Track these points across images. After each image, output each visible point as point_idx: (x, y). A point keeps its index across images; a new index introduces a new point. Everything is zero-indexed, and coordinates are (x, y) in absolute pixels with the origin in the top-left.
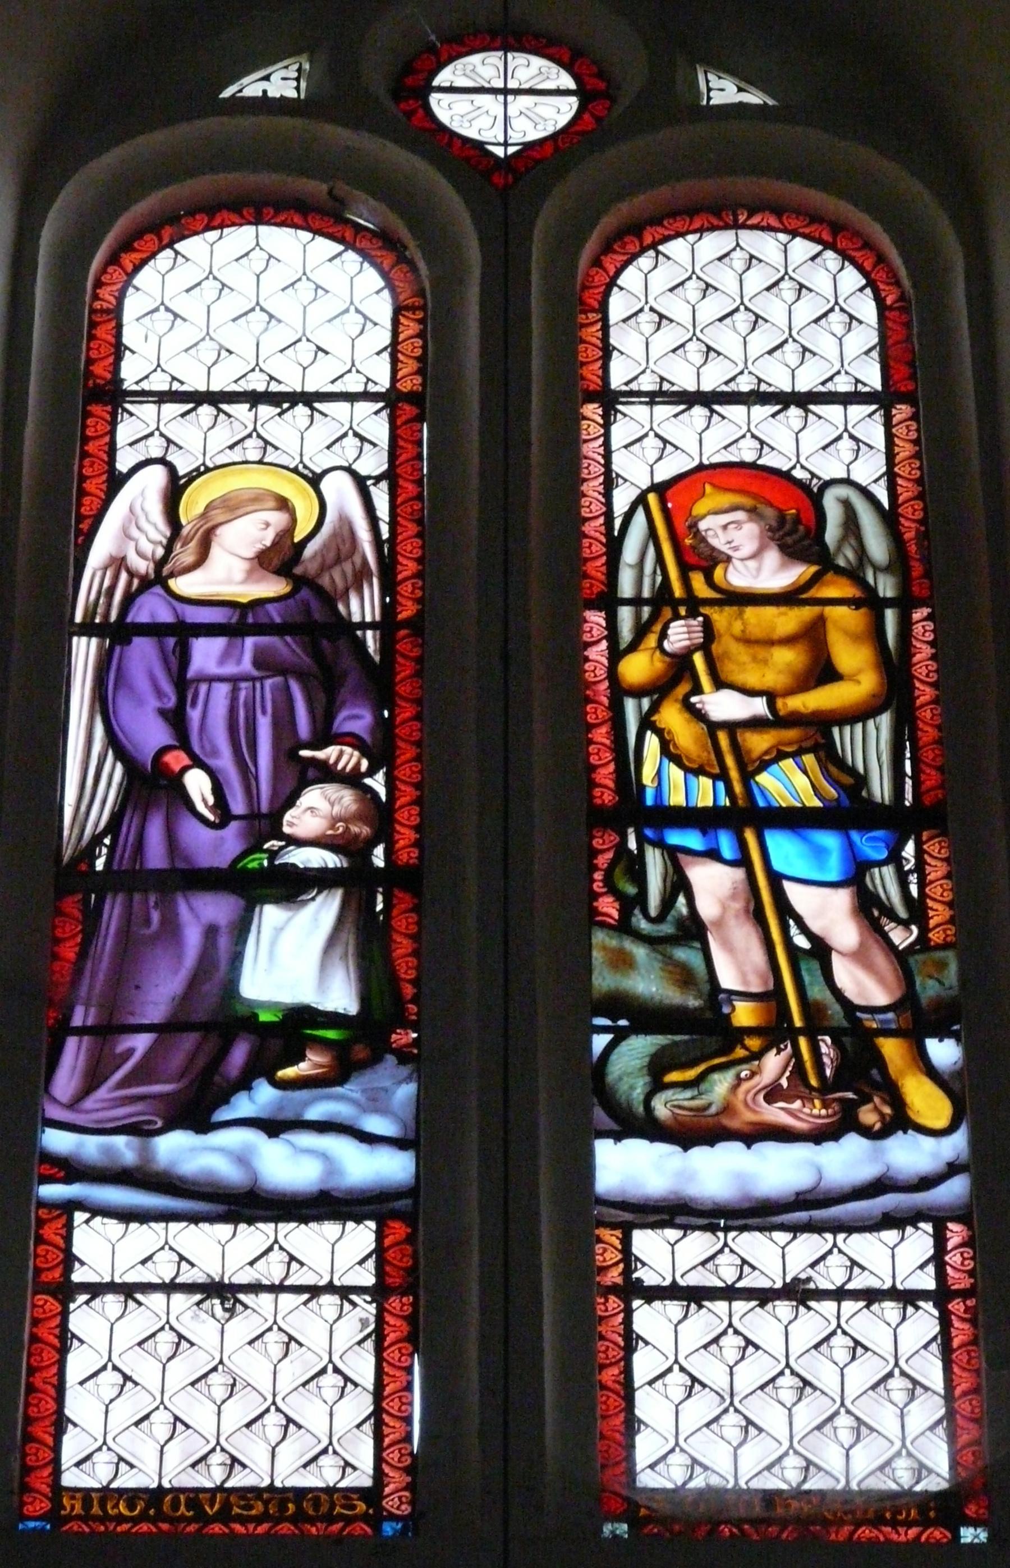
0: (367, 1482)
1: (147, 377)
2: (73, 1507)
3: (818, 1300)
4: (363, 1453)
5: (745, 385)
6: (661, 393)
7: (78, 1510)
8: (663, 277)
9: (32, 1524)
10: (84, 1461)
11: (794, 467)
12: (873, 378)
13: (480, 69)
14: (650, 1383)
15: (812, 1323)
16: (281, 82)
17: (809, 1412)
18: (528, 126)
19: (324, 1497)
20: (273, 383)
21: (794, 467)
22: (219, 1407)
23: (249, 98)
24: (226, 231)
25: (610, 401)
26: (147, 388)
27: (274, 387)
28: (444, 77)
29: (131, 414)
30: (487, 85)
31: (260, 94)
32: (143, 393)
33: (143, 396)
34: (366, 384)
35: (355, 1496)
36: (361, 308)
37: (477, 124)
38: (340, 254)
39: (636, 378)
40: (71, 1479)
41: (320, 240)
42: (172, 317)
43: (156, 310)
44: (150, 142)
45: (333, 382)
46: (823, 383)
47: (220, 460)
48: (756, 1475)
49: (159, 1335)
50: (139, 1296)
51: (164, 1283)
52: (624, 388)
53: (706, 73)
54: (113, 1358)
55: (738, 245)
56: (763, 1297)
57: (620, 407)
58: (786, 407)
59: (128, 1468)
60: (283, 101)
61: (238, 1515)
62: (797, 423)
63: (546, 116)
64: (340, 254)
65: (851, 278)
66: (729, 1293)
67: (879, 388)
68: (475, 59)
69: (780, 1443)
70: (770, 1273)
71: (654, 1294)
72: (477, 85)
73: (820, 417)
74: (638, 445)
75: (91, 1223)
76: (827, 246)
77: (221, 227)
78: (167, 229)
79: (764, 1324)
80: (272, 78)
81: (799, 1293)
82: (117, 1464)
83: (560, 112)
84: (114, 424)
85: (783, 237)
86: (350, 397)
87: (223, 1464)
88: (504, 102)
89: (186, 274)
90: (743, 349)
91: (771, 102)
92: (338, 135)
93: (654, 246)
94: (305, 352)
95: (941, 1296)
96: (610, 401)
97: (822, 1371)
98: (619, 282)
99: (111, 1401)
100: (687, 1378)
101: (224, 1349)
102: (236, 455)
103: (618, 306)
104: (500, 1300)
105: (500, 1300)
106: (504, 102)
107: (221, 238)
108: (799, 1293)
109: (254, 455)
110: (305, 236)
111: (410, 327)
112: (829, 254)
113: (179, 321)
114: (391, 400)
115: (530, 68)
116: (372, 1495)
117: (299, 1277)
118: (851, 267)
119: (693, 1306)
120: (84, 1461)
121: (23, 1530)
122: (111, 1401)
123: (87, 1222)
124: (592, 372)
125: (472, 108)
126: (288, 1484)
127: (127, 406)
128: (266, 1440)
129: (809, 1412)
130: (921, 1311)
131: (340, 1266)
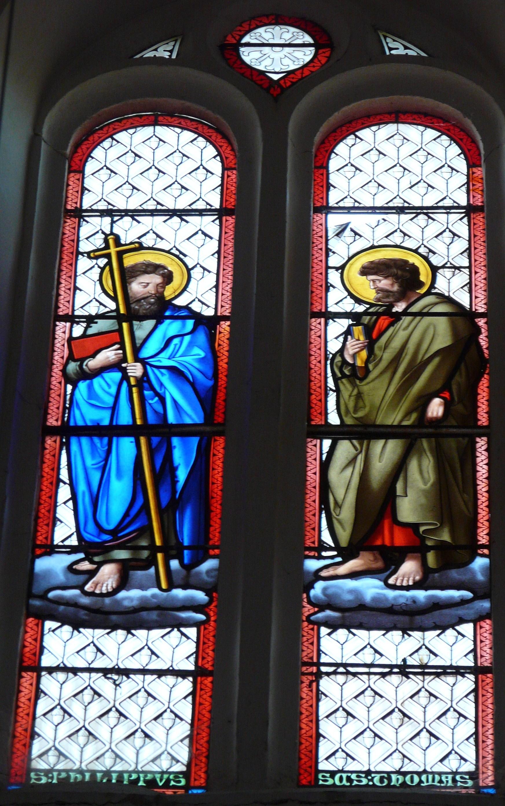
0: (472, 768)
3: (135, 674)
5: (151, 206)
7: (450, 784)
8: (117, 150)
9: (195, 791)
14: (327, 717)
15: (411, 685)
16: (163, 52)
17: (408, 730)
18: (290, 62)
20: (405, 203)
25: (79, 214)
26: (145, 208)
28: (246, 39)
29: (87, 222)
32: (144, 211)
37: (264, 64)
38: (195, 139)
39: (391, 201)
43: (198, 168)
46: (337, 203)
48: (90, 763)
55: (154, 135)
58: (418, 214)
59: (409, 761)
61: (173, 785)
62: (423, 224)
64: (195, 139)
70: (393, 657)
74: (441, 236)
77: (135, 127)
78: (350, 127)
80: (159, 50)
81: (404, 670)
83: (306, 55)
84: (79, 226)
85: (178, 130)
86: (448, 209)
88: (277, 52)
89: (361, 147)
90: (397, 189)
91: (423, 54)
92: (435, 73)
95: (197, 674)
97: (413, 709)
98: (92, 155)
101: (119, 697)
103: (90, 167)
106: (277, 52)
108: (404, 670)
110: (421, 128)
111: (234, 175)
114: (221, 213)
118: (211, 146)
123: (329, 634)
127: (86, 218)
129: (408, 730)
130: (130, 680)
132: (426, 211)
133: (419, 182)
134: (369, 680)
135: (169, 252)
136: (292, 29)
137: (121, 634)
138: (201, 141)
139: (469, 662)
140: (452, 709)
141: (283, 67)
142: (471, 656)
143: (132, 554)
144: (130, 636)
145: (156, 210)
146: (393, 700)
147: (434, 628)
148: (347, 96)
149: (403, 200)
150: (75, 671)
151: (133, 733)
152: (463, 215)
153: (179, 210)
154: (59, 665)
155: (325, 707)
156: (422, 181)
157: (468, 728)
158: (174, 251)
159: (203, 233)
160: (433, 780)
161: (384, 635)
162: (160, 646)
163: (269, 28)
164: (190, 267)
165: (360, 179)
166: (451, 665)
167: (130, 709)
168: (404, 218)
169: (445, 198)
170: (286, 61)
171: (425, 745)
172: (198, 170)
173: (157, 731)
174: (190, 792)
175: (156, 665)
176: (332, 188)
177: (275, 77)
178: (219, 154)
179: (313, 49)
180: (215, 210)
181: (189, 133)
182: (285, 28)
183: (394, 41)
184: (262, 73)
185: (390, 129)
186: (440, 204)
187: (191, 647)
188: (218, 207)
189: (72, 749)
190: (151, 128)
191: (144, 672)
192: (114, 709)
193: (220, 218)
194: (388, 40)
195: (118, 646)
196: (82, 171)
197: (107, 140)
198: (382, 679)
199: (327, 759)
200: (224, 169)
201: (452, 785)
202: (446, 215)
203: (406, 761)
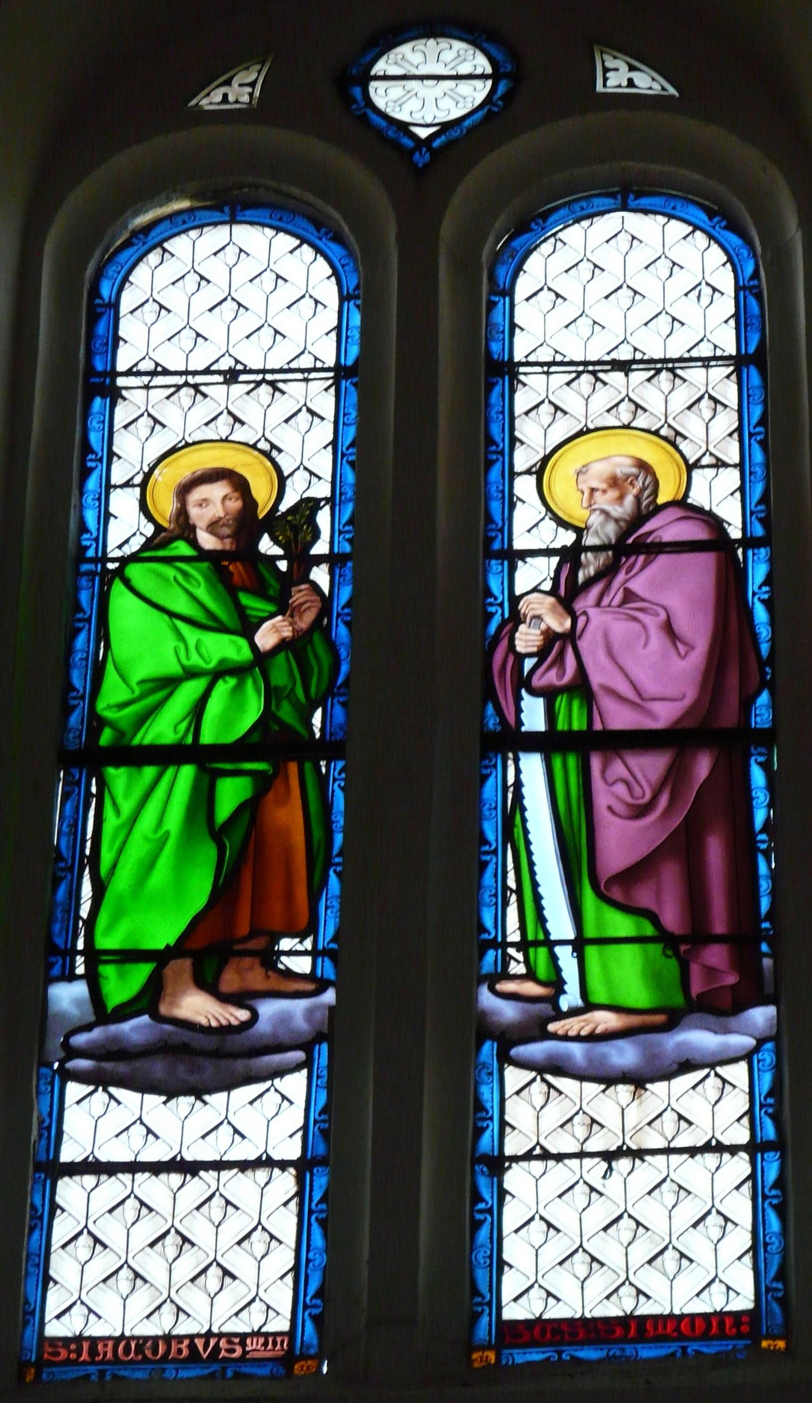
6: (715, 358)
8: (171, 269)
12: (727, 341)
15: (113, 1188)
16: (239, 90)
22: (537, 1251)
27: (719, 353)
28: (380, 67)
32: (691, 359)
35: (60, 1344)
36: (709, 282)
37: (407, 108)
39: (217, 361)
42: (632, 294)
44: (135, 151)
45: (608, 353)
47: (197, 437)
52: (524, 360)
53: (602, 53)
54: (716, 1204)
57: (522, 377)
58: (658, 371)
63: (465, 94)
68: (405, 49)
69: (529, 1279)
75: (607, 1092)
76: (303, 241)
77: (201, 226)
79: (152, 1188)
83: (478, 92)
86: (706, 362)
87: (630, 1295)
88: (430, 85)
90: (627, 327)
93: (160, 244)
99: (86, 1263)
101: (183, 1208)
102: (210, 433)
103: (523, 286)
104: (399, 1194)
105: (399, 1194)
109: (625, 418)
112: (698, 234)
113: (717, 294)
114: (739, 363)
119: (189, 1177)
121: (767, 1350)
122: (86, 1263)
126: (686, 1311)
128: (665, 1274)
131: (720, 1125)
134: (133, 1181)
136: (458, 45)
137: (185, 1102)
138: (307, 251)
140: (626, 1215)
146: (627, 1193)
148: (541, 162)
151: (205, 1270)
154: (88, 1157)
159: (309, 411)
160: (665, 1328)
161: (604, 1091)
163: (420, 44)
165: (169, 324)
167: (199, 1229)
168: (559, 379)
171: (582, 1274)
173: (697, 1244)
174: (764, 1344)
178: (730, 260)
180: (730, 357)
181: (288, 237)
182: (444, 43)
183: (615, 58)
184: (404, 127)
186: (294, 365)
187: (737, 1102)
188: (734, 353)
189: (563, 1283)
192: (173, 1231)
193: (738, 371)
195: (178, 1123)
196: (510, 292)
197: (155, 251)
198: (690, 1159)
199: (58, 1317)
200: (344, 298)
201: (88, 1359)
202: (303, 384)
203: (642, 1298)
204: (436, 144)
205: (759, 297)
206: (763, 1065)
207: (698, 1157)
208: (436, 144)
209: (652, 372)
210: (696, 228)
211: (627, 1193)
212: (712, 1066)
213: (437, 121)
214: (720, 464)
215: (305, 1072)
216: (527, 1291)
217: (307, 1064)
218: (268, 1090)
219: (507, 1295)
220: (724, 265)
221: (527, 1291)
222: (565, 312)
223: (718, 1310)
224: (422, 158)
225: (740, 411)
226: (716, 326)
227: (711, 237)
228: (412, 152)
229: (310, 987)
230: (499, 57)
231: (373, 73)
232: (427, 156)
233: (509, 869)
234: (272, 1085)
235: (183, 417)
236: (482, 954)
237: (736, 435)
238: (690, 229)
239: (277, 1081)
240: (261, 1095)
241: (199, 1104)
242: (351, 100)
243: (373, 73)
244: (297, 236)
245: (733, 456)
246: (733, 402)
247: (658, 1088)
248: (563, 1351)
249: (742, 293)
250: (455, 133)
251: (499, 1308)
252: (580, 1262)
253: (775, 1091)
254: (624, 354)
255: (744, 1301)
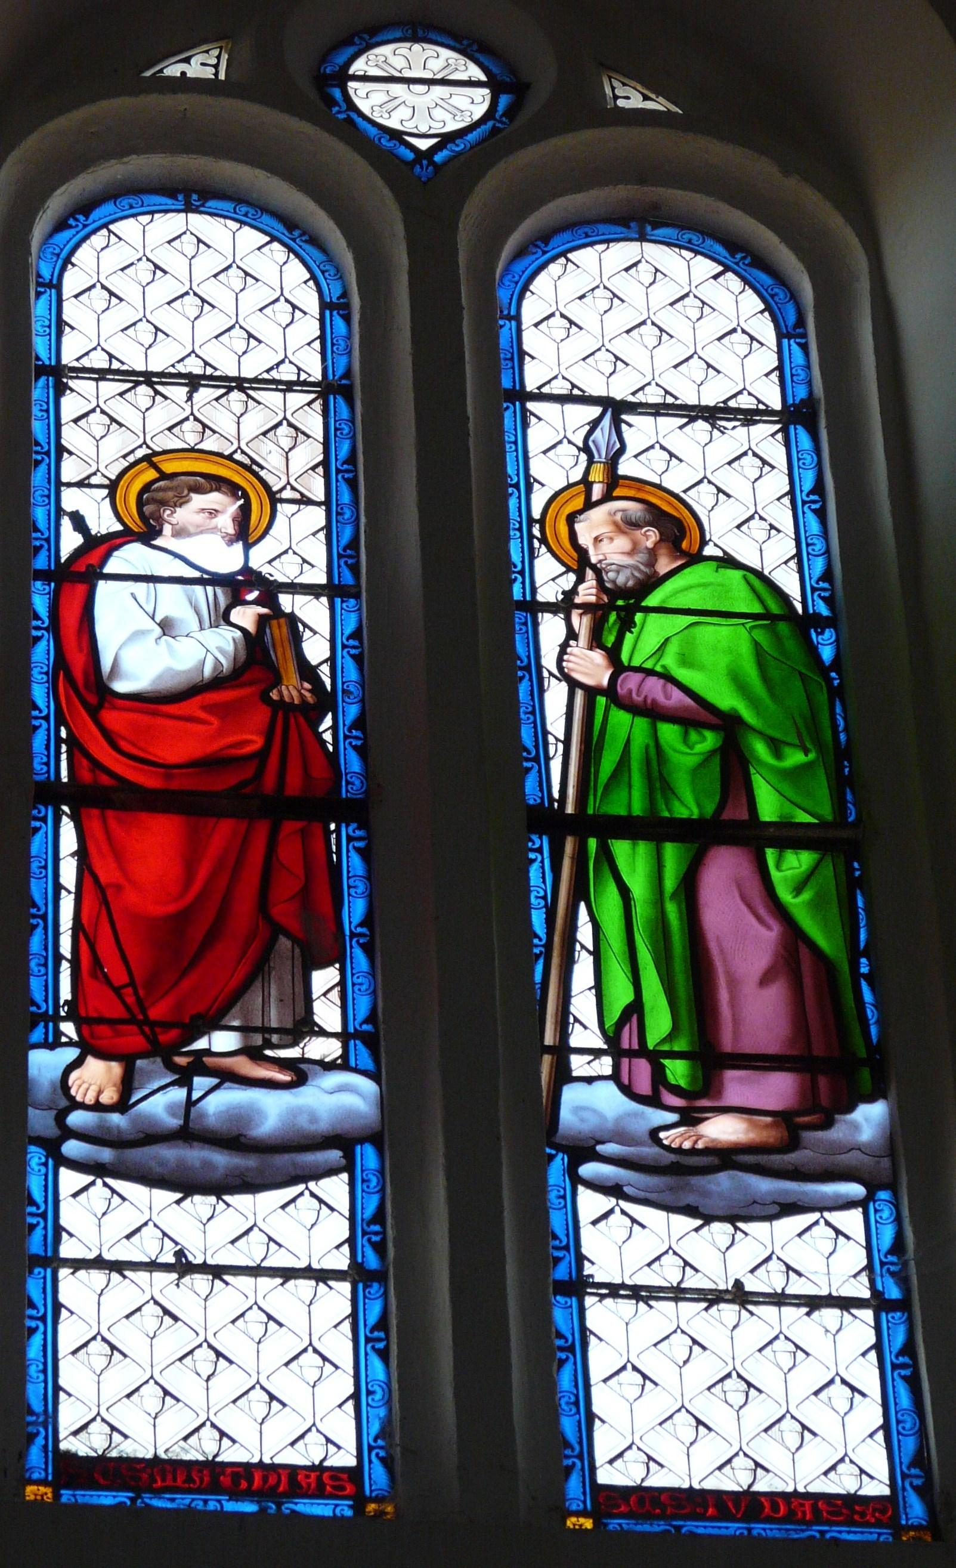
0: (351, 1462)
1: (87, 354)
2: (202, 1480)
4: (343, 1428)
10: (870, 1471)
11: (235, 452)
12: (313, 368)
13: (392, 60)
16: (200, 66)
18: (448, 117)
19: (168, 1467)
21: (235, 452)
23: (169, 77)
24: (156, 216)
25: (59, 376)
26: (88, 365)
28: (359, 67)
30: (397, 74)
31: (179, 75)
32: (274, 381)
33: (80, 372)
34: (299, 374)
35: (345, 1476)
40: (606, 1476)
41: (246, 229)
46: (77, 360)
49: (247, 1314)
50: (226, 1277)
51: (673, 1287)
52: (76, 364)
53: (610, 78)
56: (712, 1298)
60: (198, 82)
62: (238, 408)
65: (752, 302)
66: (678, 1294)
67: (320, 378)
68: (386, 50)
70: (713, 1274)
71: (78, 1265)
72: (385, 74)
73: (259, 403)
80: (193, 61)
82: (755, 1471)
83: (473, 105)
85: (234, 226)
86: (289, 387)
88: (420, 93)
91: (674, 109)
94: (604, 361)
96: (59, 376)
100: (639, 1376)
101: (212, 1331)
103: (531, 309)
104: (470, 1303)
105: (470, 1303)
106: (420, 93)
107: (152, 221)
109: (192, 439)
112: (276, 245)
115: (438, 59)
116: (354, 1474)
117: (798, 1287)
118: (297, 260)
120: (870, 1471)
124: (41, 347)
125: (387, 99)
132: (693, 413)
133: (691, 357)
135: (230, 457)
136: (445, 53)
138: (732, 281)
139: (341, 1261)
141: (434, 124)
142: (864, 1278)
143: (245, 1038)
144: (739, 1235)
145: (109, 371)
147: (690, 1211)
149: (571, 383)
150: (119, 1267)
152: (313, 396)
153: (707, 408)
155: (69, 1333)
156: (696, 356)
157: (870, 1413)
158: (238, 456)
162: (281, 1225)
163: (403, 48)
164: (64, 479)
166: (830, 1294)
169: (740, 393)
170: (438, 113)
172: (277, 304)
175: (279, 1260)
176: (67, 329)
177: (424, 144)
179: (486, 91)
182: (431, 49)
183: (624, 84)
185: (624, 252)
187: (854, 1256)
190: (636, 245)
191: (256, 1271)
194: (616, 83)
200: (780, 336)
203: (226, 1442)
204: (438, 158)
205: (347, 319)
206: (368, 1187)
207: (82, 1273)
208: (438, 158)
209: (222, 391)
210: (274, 239)
211: (734, 1353)
212: (821, 1210)
213: (432, 132)
214: (305, 501)
215: (345, 1176)
216: (197, 1430)
217: (349, 1167)
218: (301, 1194)
219: (601, 1454)
220: (762, 312)
221: (197, 1430)
222: (121, 315)
223: (852, 1492)
224: (422, 172)
225: (326, 444)
226: (296, 341)
227: (290, 250)
228: (411, 165)
229: (284, 1077)
230: (495, 70)
231: (351, 72)
232: (431, 168)
233: (62, 929)
234: (307, 1188)
235: (158, 421)
236: (34, 1025)
237: (320, 470)
238: (268, 239)
239: (312, 1185)
240: (293, 1200)
241: (221, 1206)
242: (331, 102)
243: (351, 72)
244: (720, 263)
245: (319, 495)
246: (318, 432)
247: (757, 1229)
248: (283, 1503)
249: (328, 313)
250: (460, 146)
251: (593, 1469)
252: (151, 1395)
253: (898, 1247)
254: (194, 367)
255: (878, 1488)
